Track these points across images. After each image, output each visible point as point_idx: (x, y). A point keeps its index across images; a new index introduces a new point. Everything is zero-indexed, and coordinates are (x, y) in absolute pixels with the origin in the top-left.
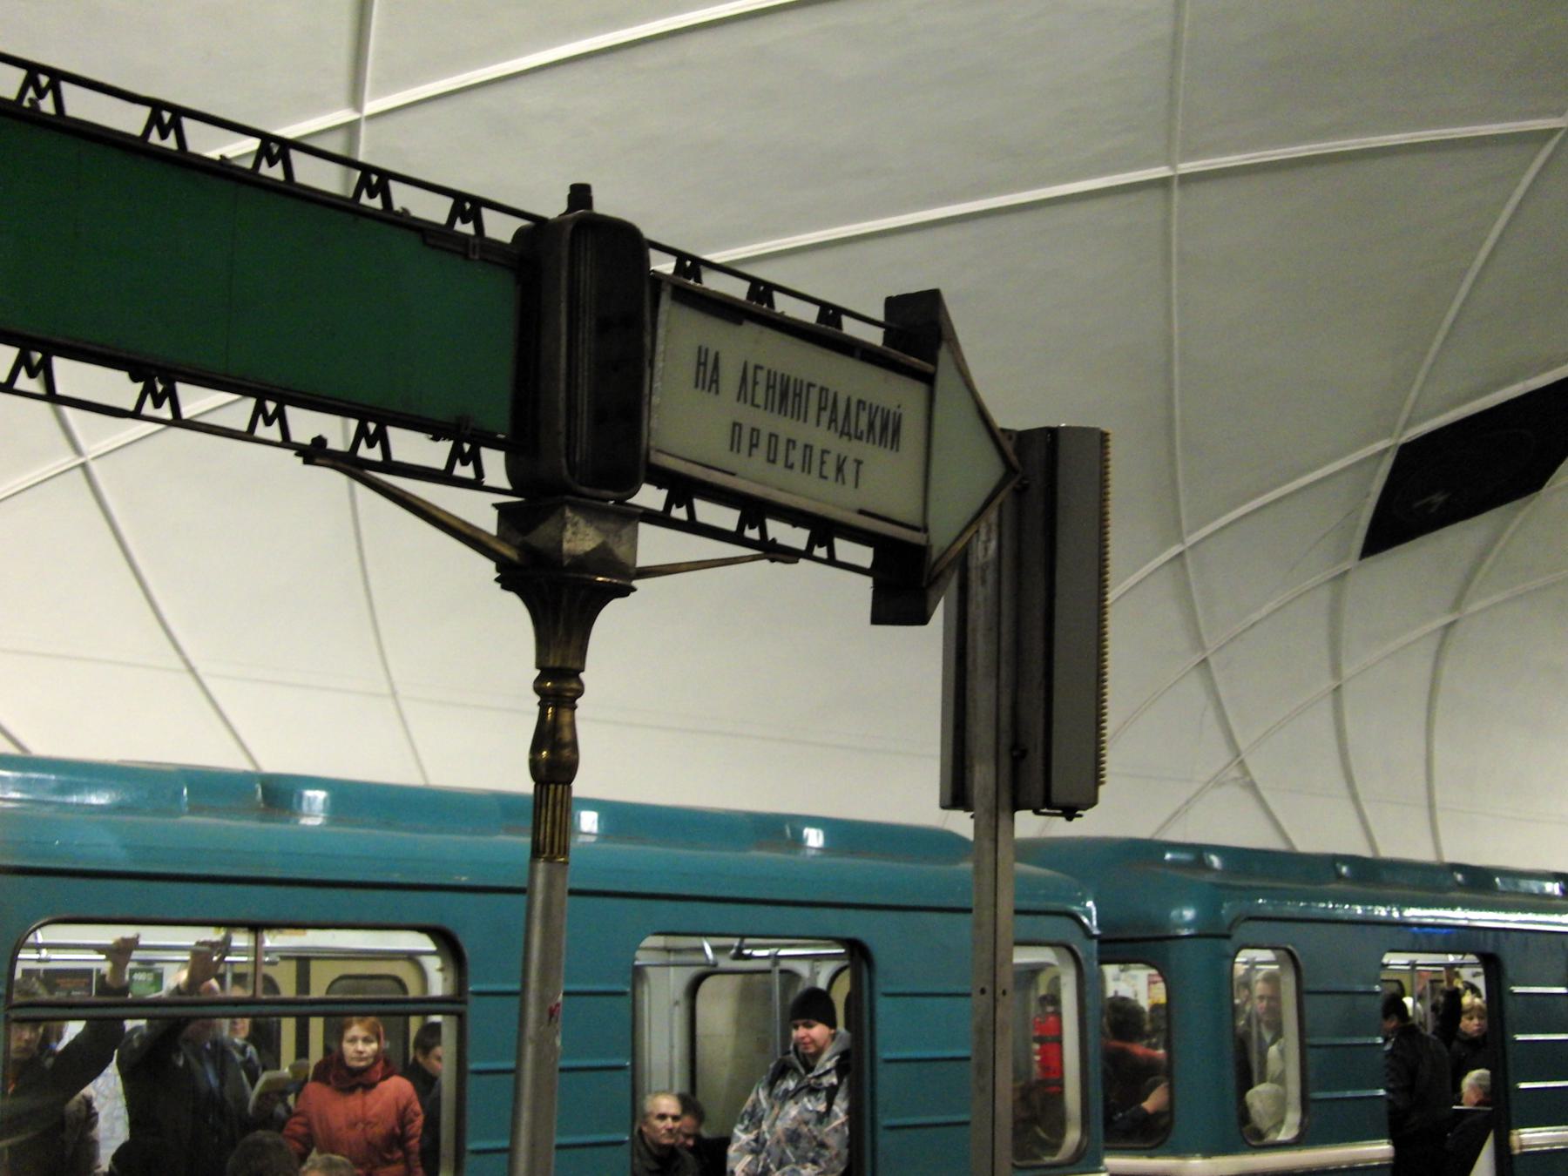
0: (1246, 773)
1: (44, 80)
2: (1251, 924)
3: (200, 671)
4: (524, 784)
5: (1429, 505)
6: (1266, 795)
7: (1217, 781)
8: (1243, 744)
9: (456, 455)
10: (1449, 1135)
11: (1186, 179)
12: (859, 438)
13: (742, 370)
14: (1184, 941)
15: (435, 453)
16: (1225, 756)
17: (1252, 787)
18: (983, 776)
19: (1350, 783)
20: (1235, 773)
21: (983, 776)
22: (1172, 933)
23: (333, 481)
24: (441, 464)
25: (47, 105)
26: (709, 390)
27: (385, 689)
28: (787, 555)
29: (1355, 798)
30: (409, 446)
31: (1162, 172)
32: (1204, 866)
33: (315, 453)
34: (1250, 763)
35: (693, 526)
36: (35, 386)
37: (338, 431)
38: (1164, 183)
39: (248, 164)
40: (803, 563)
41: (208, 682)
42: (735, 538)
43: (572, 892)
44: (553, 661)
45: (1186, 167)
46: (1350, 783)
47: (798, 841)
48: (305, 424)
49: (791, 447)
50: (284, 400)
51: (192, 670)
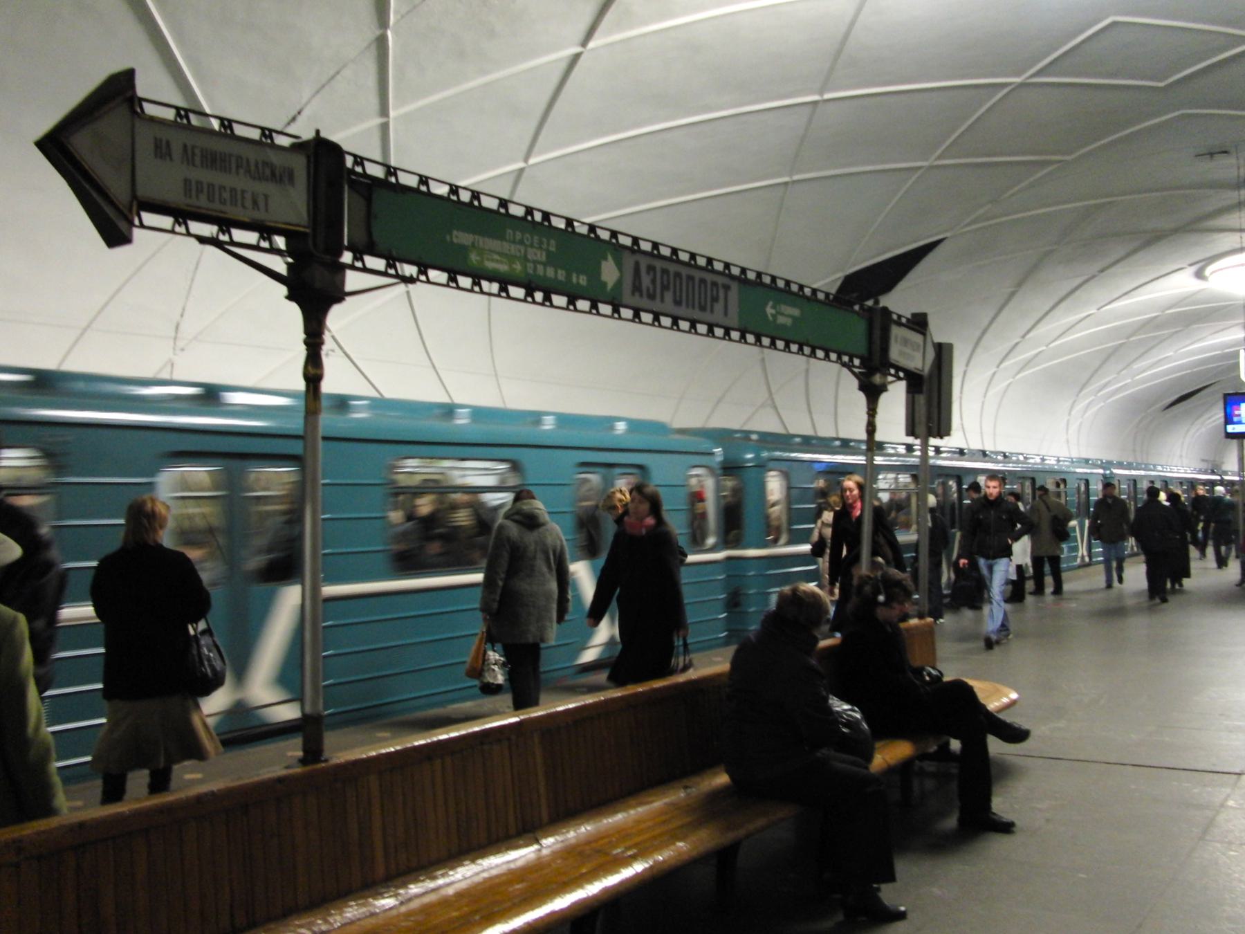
0: (774, 402)
1: (226, 123)
2: (773, 462)
3: (437, 368)
4: (300, 385)
5: (586, 481)
6: (781, 411)
7: (763, 406)
8: (773, 391)
9: (389, 265)
10: (1099, 522)
11: (794, 182)
12: (267, 180)
13: (1169, 409)
14: (750, 469)
15: (251, 237)
16: (767, 395)
17: (775, 408)
18: (921, 429)
19: (809, 405)
20: (769, 402)
21: (921, 429)
22: (742, 465)
23: (211, 250)
24: (169, 227)
25: (393, 180)
26: (237, 173)
27: (1235, 776)
28: (410, 280)
29: (810, 412)
30: (239, 235)
31: (786, 179)
32: (748, 439)
33: (202, 240)
34: (774, 396)
35: (365, 270)
36: (454, 285)
37: (208, 230)
38: (786, 184)
39: (446, 195)
40: (418, 283)
41: (439, 371)
42: (385, 274)
43: (325, 438)
44: (871, 407)
45: (796, 177)
46: (809, 405)
47: (612, 428)
48: (197, 228)
49: (651, 291)
50: (395, 260)
51: (434, 367)
